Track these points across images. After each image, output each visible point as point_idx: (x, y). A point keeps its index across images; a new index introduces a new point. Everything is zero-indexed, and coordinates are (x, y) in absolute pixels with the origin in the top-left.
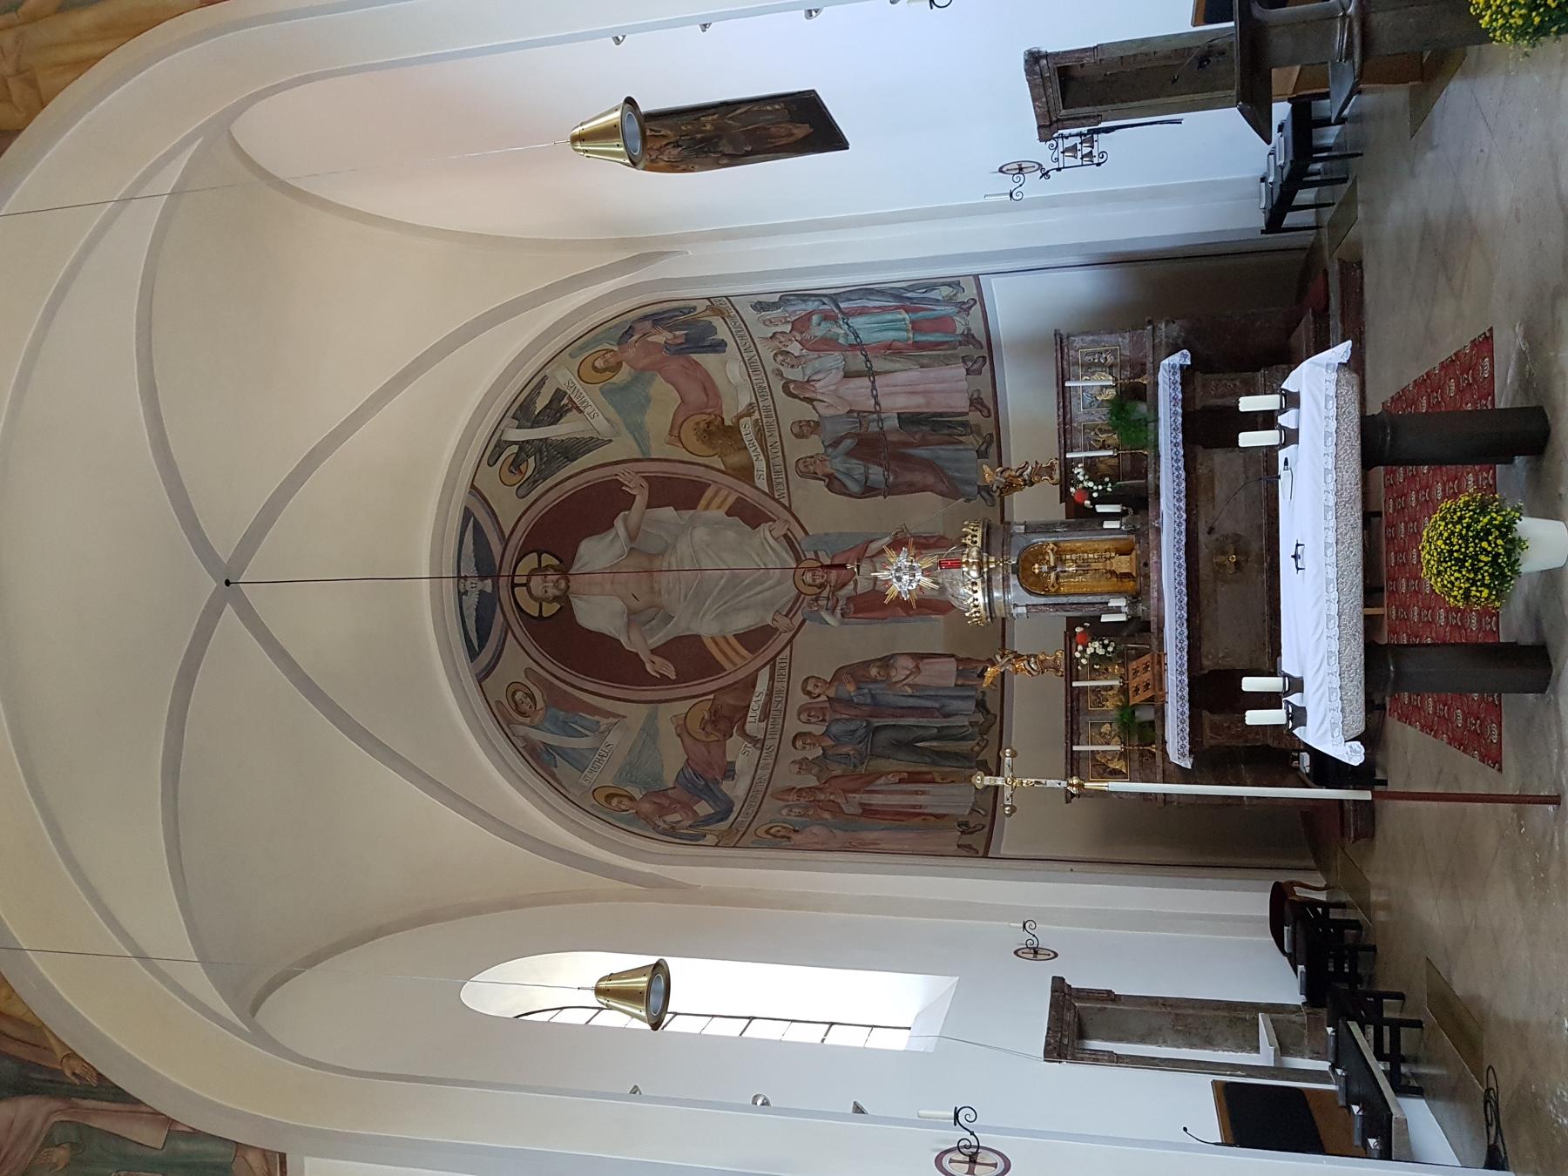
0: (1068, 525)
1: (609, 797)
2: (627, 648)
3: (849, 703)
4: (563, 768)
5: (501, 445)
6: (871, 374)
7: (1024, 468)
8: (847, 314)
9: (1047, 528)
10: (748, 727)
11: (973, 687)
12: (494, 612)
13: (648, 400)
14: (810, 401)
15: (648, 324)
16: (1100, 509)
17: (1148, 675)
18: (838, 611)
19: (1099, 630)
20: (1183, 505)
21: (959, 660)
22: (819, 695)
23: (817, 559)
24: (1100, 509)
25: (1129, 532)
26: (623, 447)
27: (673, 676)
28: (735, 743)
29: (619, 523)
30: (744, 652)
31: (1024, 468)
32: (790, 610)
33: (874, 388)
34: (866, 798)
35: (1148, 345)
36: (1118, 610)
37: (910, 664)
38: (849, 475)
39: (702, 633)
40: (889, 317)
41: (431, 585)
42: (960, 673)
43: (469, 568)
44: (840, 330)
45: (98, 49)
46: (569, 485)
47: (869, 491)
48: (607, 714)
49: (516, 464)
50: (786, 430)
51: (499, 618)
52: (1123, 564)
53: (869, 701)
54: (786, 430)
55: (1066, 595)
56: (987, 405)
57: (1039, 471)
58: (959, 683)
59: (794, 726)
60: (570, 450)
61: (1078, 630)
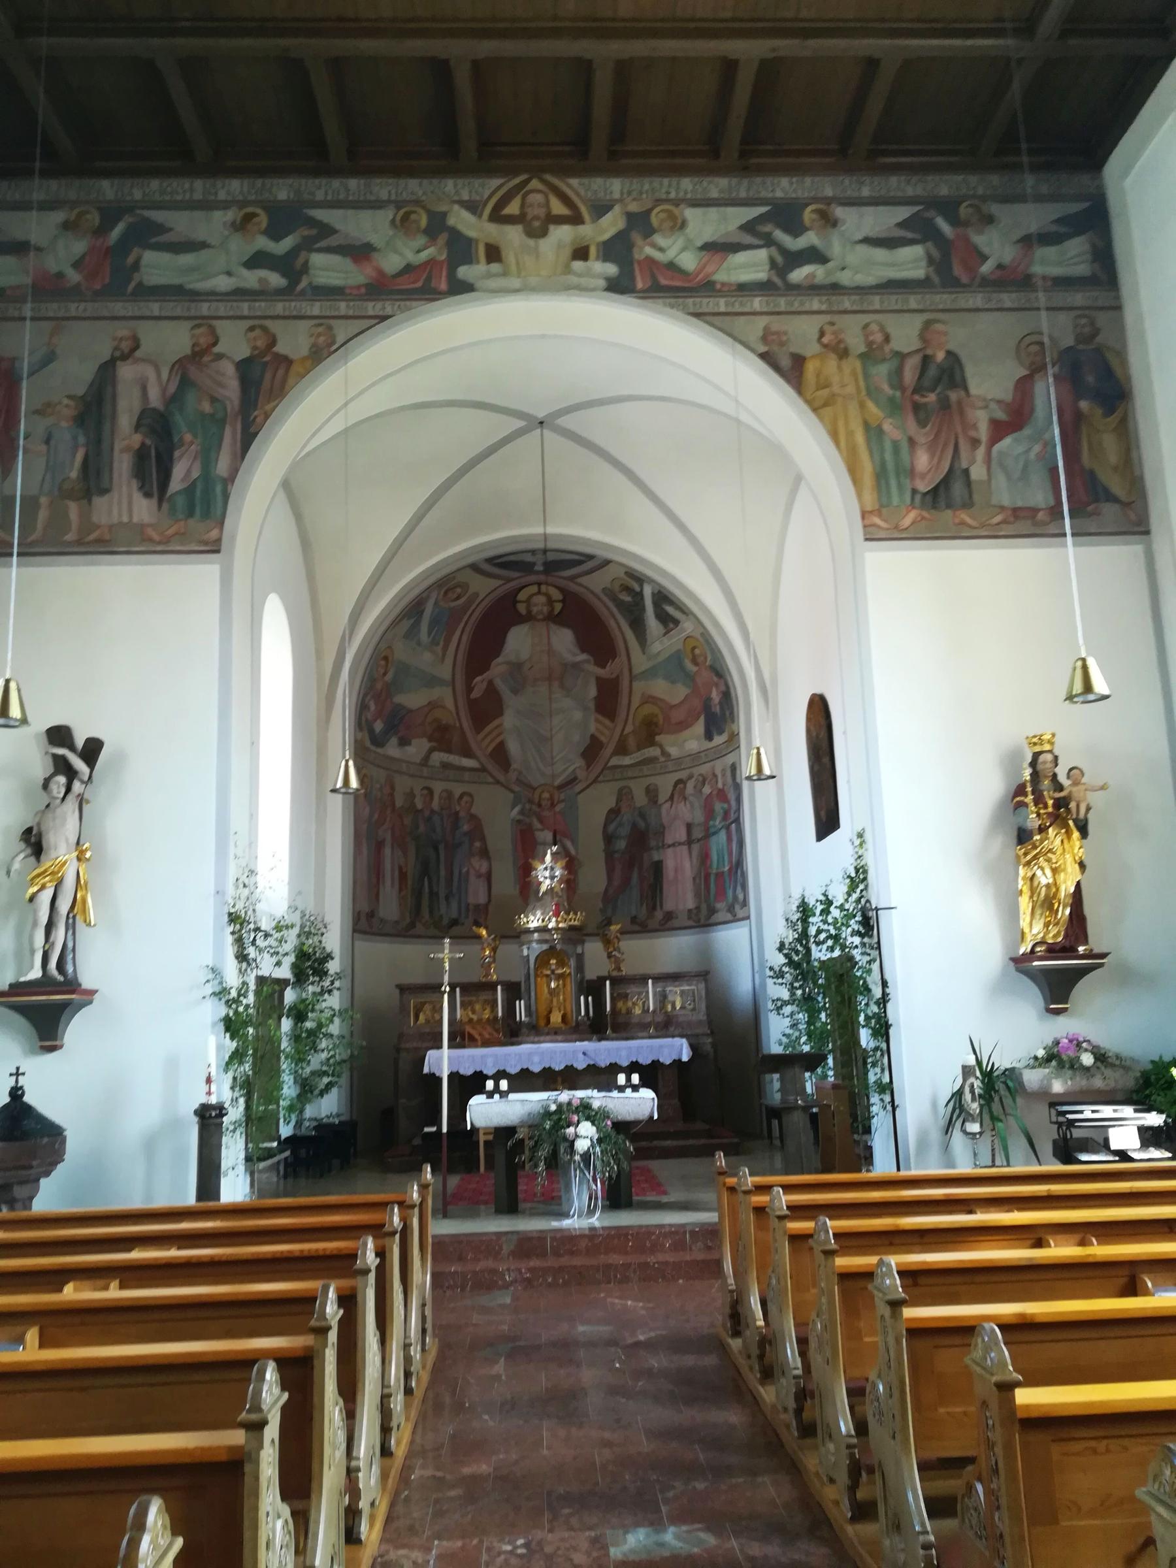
1: (386, 658)
4: (406, 624)
6: (689, 842)
9: (580, 968)
11: (467, 917)
13: (673, 682)
14: (671, 798)
15: (723, 688)
18: (521, 817)
23: (559, 802)
26: (640, 662)
27: (474, 695)
29: (584, 656)
30: (490, 749)
33: (680, 844)
37: (484, 870)
40: (726, 857)
41: (540, 535)
42: (477, 907)
43: (551, 557)
44: (718, 822)
45: (843, 444)
47: (609, 839)
48: (444, 655)
49: (627, 589)
50: (652, 780)
51: (516, 574)
52: (556, 1018)
54: (652, 780)
56: (669, 924)
59: (438, 787)
60: (638, 625)
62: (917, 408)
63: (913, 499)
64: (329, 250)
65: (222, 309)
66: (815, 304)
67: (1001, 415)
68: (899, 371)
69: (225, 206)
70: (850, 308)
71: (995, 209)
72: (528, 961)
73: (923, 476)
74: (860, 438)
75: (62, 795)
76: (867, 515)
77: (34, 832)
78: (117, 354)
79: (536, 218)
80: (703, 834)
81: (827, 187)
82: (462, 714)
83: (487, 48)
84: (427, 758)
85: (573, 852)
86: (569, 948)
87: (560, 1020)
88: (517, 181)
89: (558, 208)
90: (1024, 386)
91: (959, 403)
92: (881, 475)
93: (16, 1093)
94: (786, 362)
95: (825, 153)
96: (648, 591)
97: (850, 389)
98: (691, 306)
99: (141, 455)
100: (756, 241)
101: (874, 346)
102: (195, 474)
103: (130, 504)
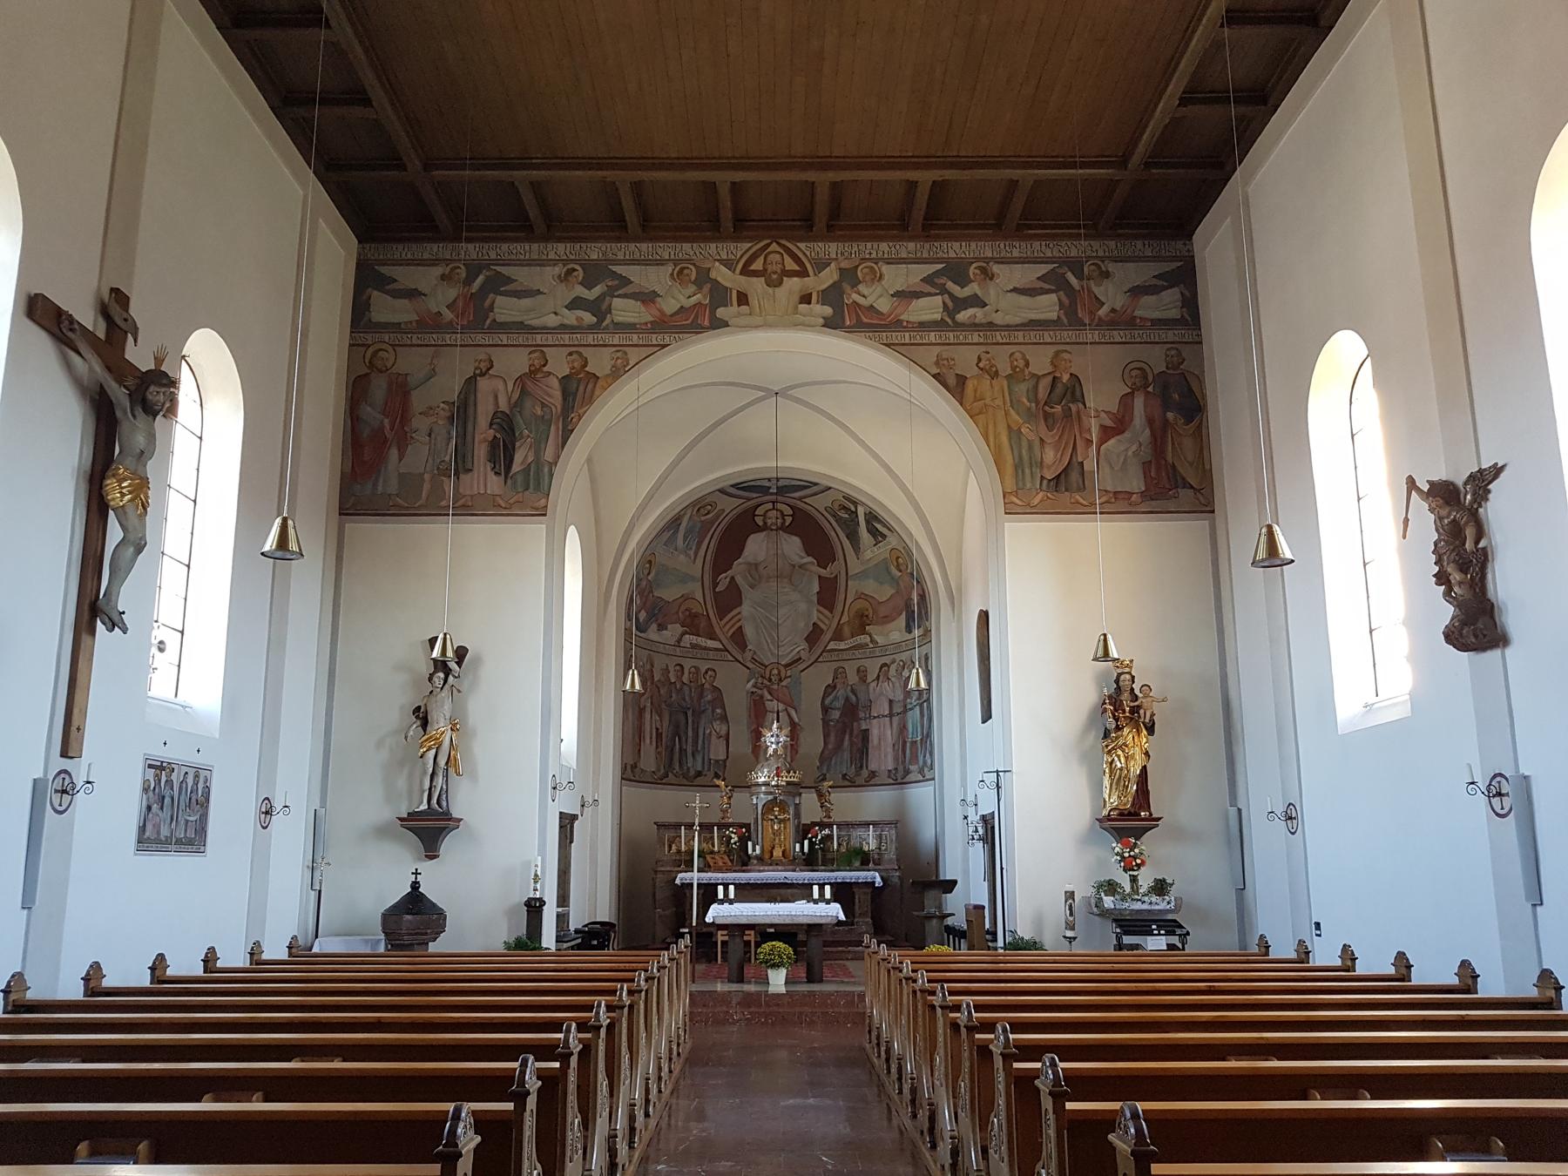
0: (798, 826)
1: (650, 562)
2: (735, 563)
3: (701, 696)
4: (667, 535)
5: (855, 503)
6: (891, 715)
7: (830, 803)
8: (921, 705)
9: (797, 815)
10: (687, 636)
12: (759, 493)
13: (881, 583)
14: (878, 678)
16: (806, 842)
17: (721, 864)
18: (754, 690)
19: (743, 841)
20: (806, 881)
21: (725, 761)
22: (705, 678)
23: (786, 678)
24: (806, 842)
25: (794, 856)
26: (855, 566)
27: (717, 590)
28: (679, 629)
29: (810, 559)
31: (830, 803)
32: (756, 661)
33: (883, 716)
34: (648, 710)
35: (888, 867)
36: (754, 850)
37: (723, 732)
38: (836, 698)
39: (743, 607)
40: (919, 729)
42: (717, 761)
43: (781, 483)
45: (992, 444)
46: (833, 533)
47: (826, 710)
51: (755, 495)
52: (777, 853)
53: (703, 708)
55: (762, 823)
56: (871, 780)
57: (828, 811)
58: (712, 762)
60: (853, 537)
61: (744, 830)
62: (1047, 416)
63: (1041, 484)
64: (625, 296)
65: (550, 339)
66: (976, 338)
67: (1109, 423)
68: (1036, 387)
69: (554, 262)
70: (1001, 341)
71: (1111, 267)
72: (757, 808)
73: (1049, 467)
74: (1004, 439)
75: (441, 686)
76: (1007, 496)
77: (422, 711)
78: (478, 372)
79: (775, 273)
80: (902, 709)
81: (987, 249)
82: (709, 606)
83: (740, 176)
84: (679, 641)
85: (796, 720)
86: (789, 800)
87: (781, 854)
88: (762, 244)
89: (790, 265)
90: (1126, 401)
91: (1078, 412)
92: (1018, 466)
93: (415, 886)
94: (952, 381)
95: (984, 227)
96: (861, 511)
97: (999, 402)
98: (884, 338)
99: (494, 444)
100: (933, 290)
101: (1018, 369)
102: (530, 459)
103: (486, 479)
